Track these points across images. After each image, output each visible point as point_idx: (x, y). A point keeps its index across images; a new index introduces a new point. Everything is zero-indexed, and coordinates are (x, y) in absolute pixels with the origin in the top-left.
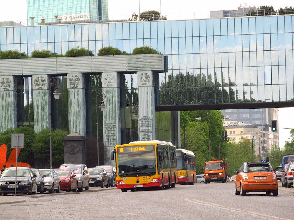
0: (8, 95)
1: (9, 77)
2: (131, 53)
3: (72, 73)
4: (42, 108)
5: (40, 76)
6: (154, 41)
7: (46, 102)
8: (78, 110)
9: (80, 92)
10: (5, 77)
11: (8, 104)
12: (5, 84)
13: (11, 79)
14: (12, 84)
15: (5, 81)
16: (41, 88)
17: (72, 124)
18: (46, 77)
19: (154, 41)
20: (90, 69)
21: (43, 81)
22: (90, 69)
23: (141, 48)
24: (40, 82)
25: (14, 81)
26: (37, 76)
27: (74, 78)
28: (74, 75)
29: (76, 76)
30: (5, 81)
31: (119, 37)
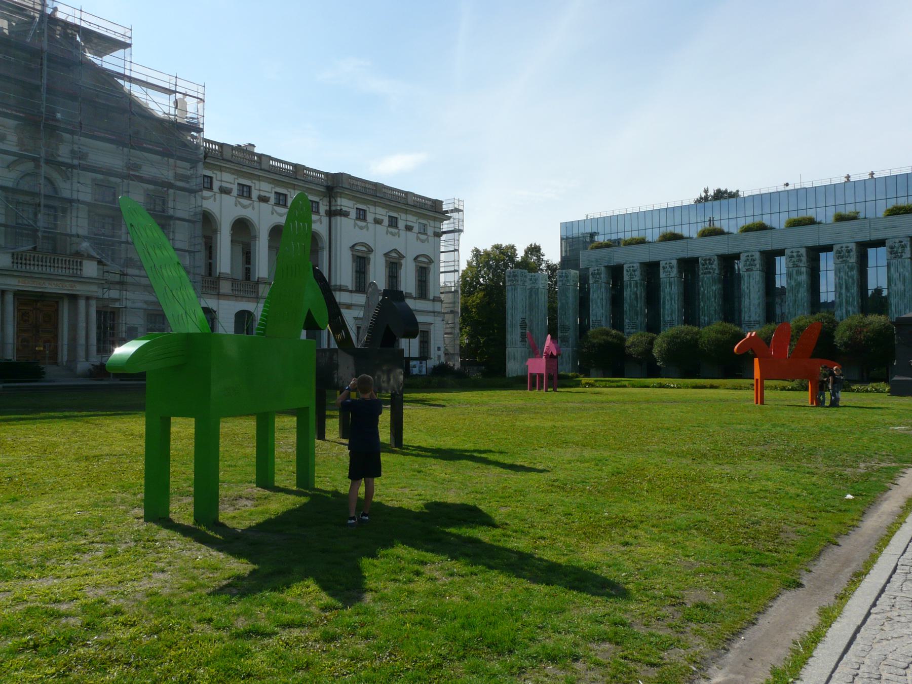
0: (799, 273)
1: (799, 249)
2: (783, 227)
3: (894, 237)
4: (846, 287)
5: (844, 245)
6: (686, 228)
7: (853, 279)
8: (902, 288)
9: (906, 264)
10: (795, 250)
11: (799, 284)
12: (794, 259)
13: (803, 251)
14: (804, 259)
15: (795, 254)
16: (846, 262)
17: (893, 308)
18: (853, 246)
19: (686, 228)
20: (88, 306)
21: (849, 251)
22: (88, 306)
23: (795, 220)
24: (844, 252)
25: (807, 256)
26: (839, 246)
27: (897, 245)
28: (897, 240)
29: (901, 242)
30: (795, 254)
31: (642, 227)
